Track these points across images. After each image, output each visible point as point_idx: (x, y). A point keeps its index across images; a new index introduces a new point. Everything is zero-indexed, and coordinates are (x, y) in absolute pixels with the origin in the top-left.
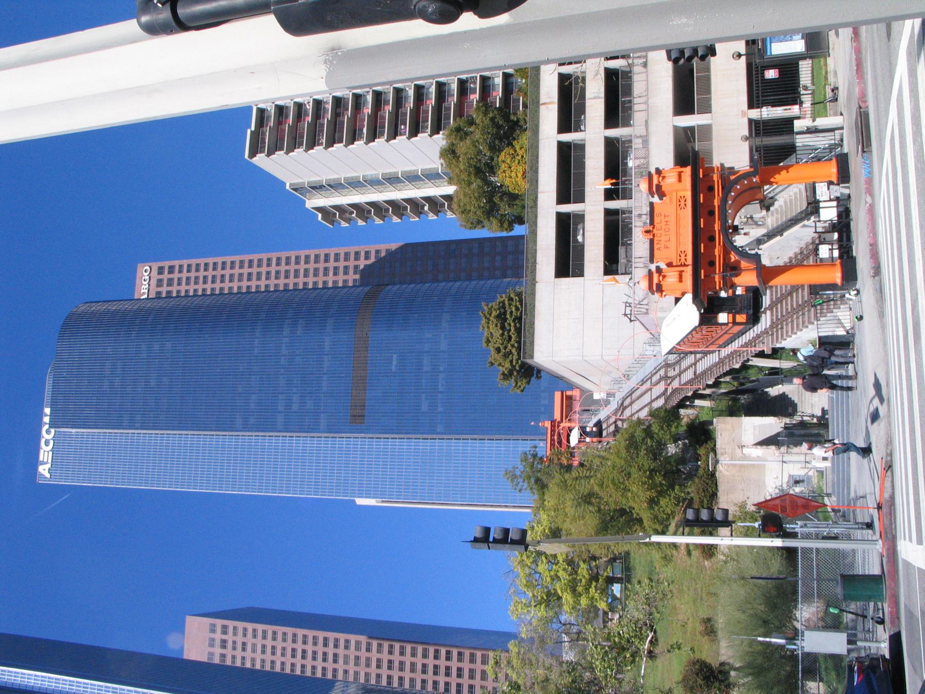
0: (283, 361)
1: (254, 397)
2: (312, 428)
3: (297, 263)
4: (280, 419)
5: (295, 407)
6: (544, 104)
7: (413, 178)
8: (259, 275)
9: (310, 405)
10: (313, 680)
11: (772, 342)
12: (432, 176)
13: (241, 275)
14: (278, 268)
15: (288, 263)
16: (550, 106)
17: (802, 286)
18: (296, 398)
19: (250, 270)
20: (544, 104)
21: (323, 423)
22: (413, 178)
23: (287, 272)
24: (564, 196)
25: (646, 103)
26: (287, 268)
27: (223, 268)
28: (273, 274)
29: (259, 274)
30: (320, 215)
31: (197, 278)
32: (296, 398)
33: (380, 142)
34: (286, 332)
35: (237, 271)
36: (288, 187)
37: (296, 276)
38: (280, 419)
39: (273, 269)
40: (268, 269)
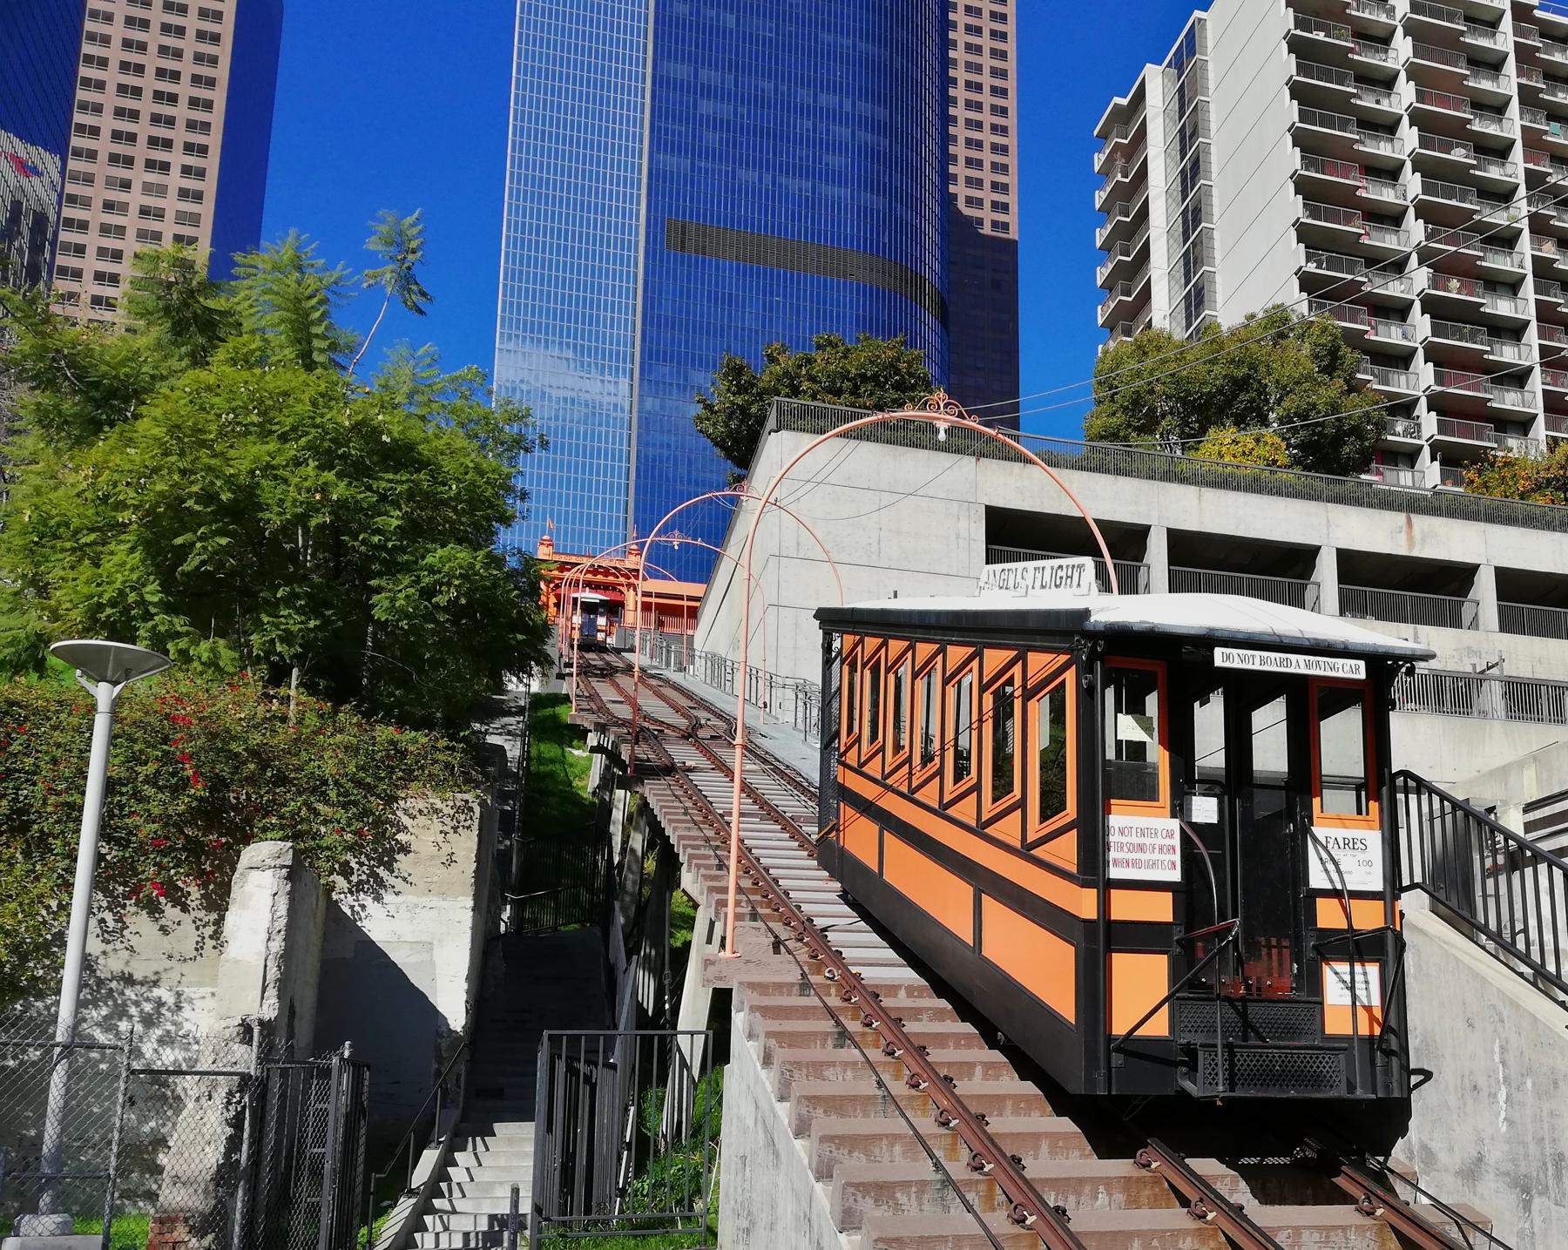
0: (804, 95)
1: (731, 20)
2: (659, 142)
3: (995, 186)
4: (682, 71)
5: (706, 107)
6: (1409, 519)
7: (1193, 260)
8: (976, 183)
9: (711, 138)
10: (67, 103)
11: (761, 988)
12: (1196, 300)
13: (979, 164)
14: (987, 146)
15: (995, 167)
16: (1403, 537)
17: (899, 987)
18: (726, 110)
19: (987, 166)
20: (1409, 519)
21: (671, 161)
22: (1193, 260)
23: (979, 164)
24: (1354, 566)
25: (1246, 693)
26: (987, 166)
27: (994, 33)
28: (976, 135)
29: (978, 106)
30: (1124, 102)
31: (978, 31)
32: (726, 110)
33: (1295, 207)
34: (864, 107)
35: (987, 61)
36: (1197, 14)
37: (969, 104)
38: (682, 71)
39: (987, 137)
40: (987, 127)
